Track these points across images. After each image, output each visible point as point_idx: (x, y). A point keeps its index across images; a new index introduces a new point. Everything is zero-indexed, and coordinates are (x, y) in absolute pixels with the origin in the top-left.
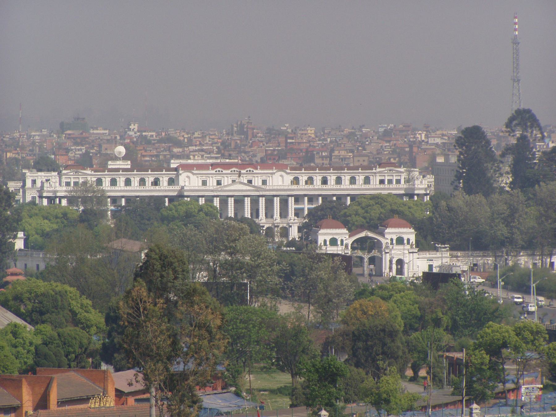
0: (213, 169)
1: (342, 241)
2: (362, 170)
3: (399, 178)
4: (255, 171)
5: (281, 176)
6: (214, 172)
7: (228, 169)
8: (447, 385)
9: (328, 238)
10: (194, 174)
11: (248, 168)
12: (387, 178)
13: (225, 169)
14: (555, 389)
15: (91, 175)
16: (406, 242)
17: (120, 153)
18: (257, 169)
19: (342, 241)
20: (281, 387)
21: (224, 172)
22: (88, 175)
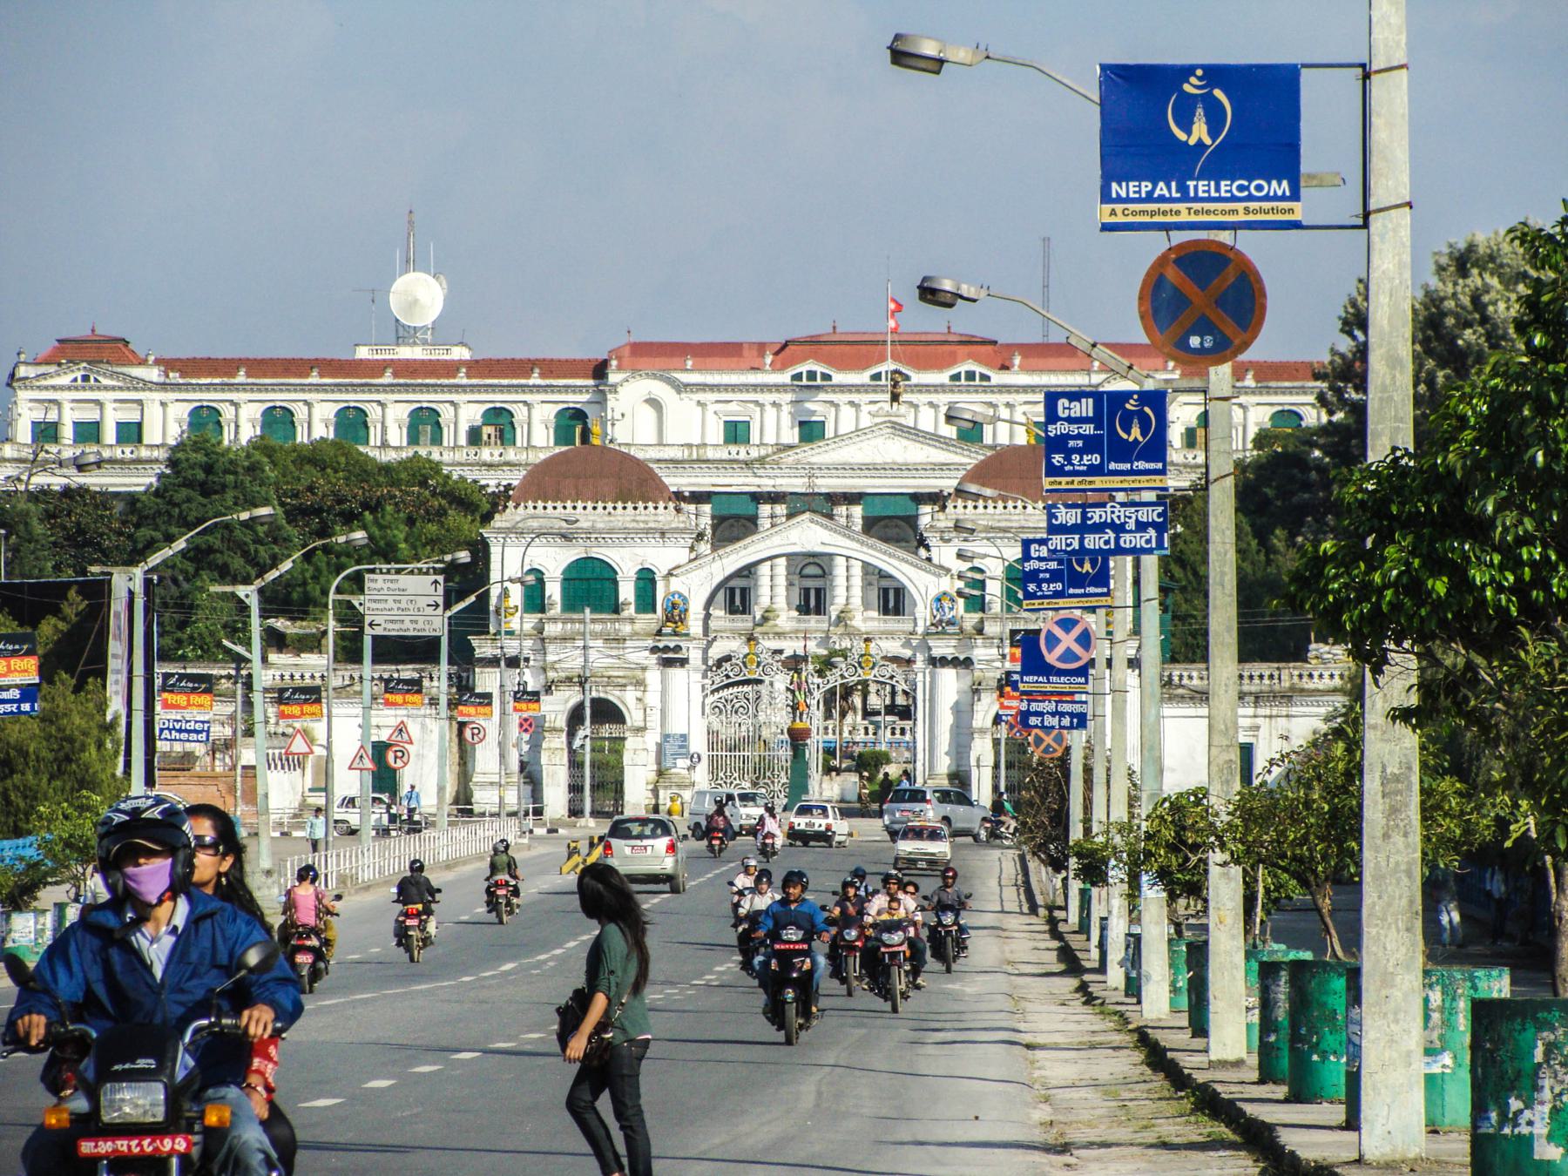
0: (778, 367)
1: (646, 580)
2: (248, 375)
3: (134, 416)
4: (997, 378)
5: (654, 403)
6: (785, 378)
7: (938, 364)
8: (437, 640)
9: (554, 561)
10: (681, 388)
11: (804, 359)
12: (69, 417)
13: (843, 366)
14: (25, 571)
15: (163, 386)
16: (627, 592)
18: (1005, 367)
19: (646, 580)
20: (1423, 802)
21: (839, 378)
22: (147, 385)
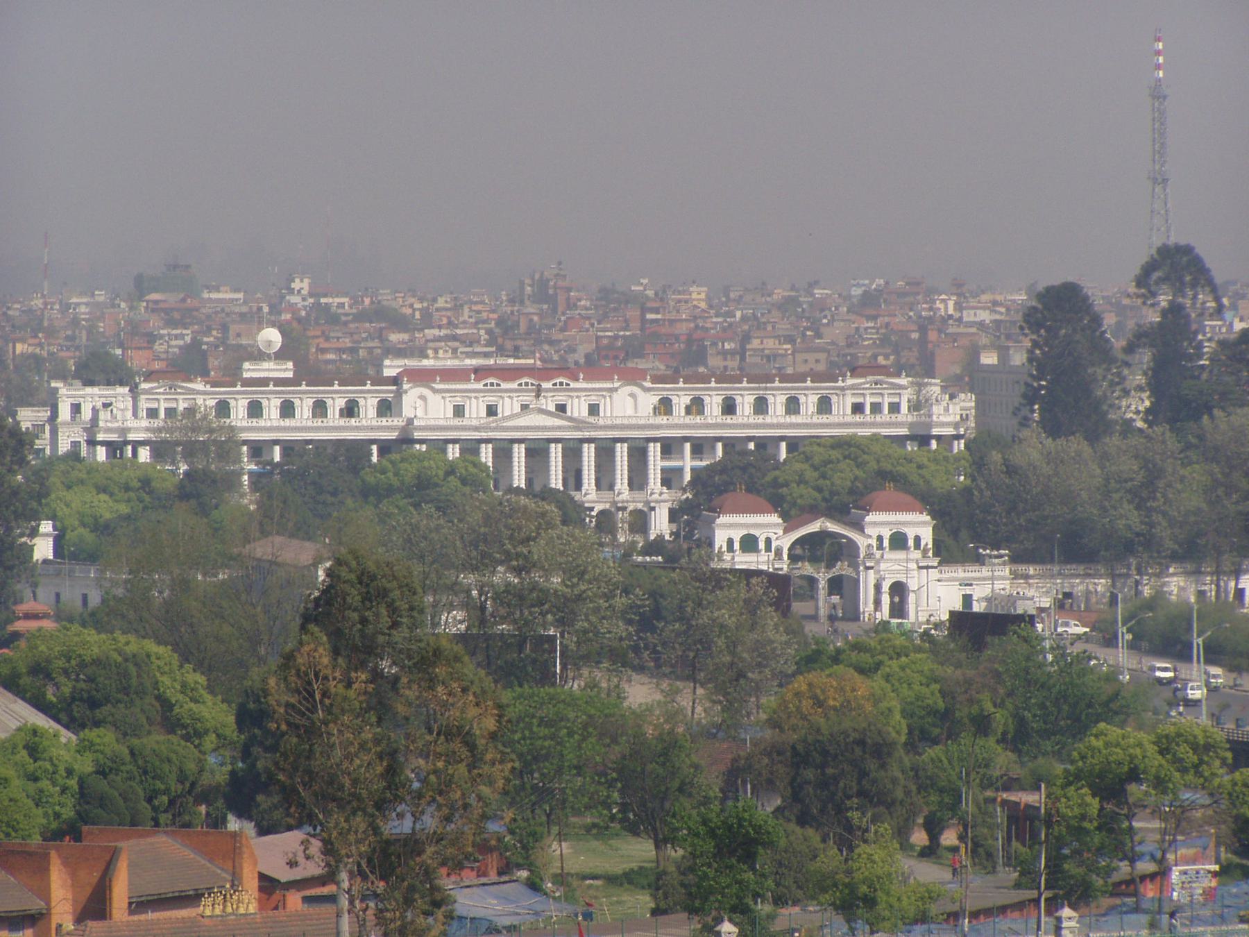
0: (477, 380)
1: (768, 542)
2: (812, 381)
3: (896, 400)
4: (573, 385)
5: (632, 395)
6: (480, 386)
7: (513, 379)
8: (1004, 865)
9: (737, 535)
10: (435, 391)
11: (558, 376)
12: (869, 400)
13: (505, 380)
14: (1248, 874)
15: (205, 393)
16: (911, 543)
17: (269, 343)
18: (577, 380)
19: (768, 542)
20: (632, 870)
21: (504, 386)
22: (199, 393)
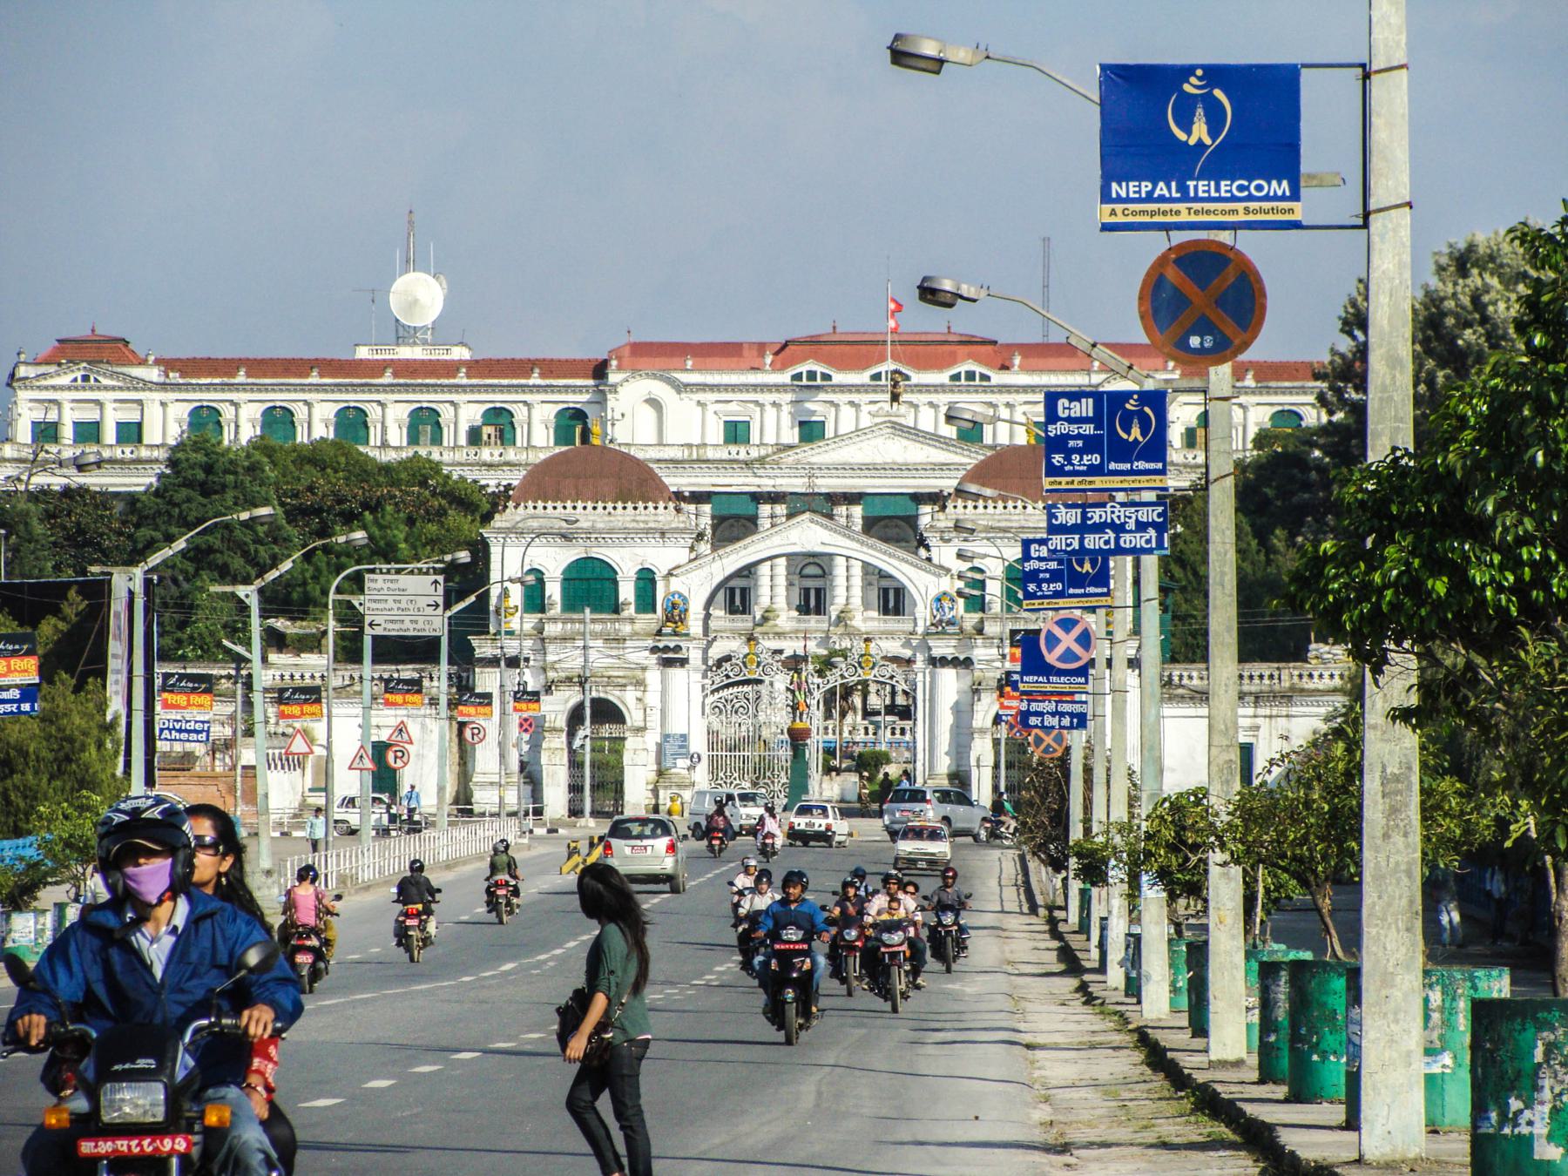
0: (778, 367)
1: (646, 580)
2: (248, 375)
3: (134, 416)
4: (997, 378)
5: (654, 403)
6: (785, 378)
7: (938, 364)
8: (437, 640)
9: (554, 561)
10: (681, 388)
11: (804, 359)
12: (69, 417)
13: (843, 366)
14: (25, 571)
15: (163, 386)
17: (413, 304)
18: (1005, 367)
19: (646, 580)
21: (839, 378)
22: (147, 385)
